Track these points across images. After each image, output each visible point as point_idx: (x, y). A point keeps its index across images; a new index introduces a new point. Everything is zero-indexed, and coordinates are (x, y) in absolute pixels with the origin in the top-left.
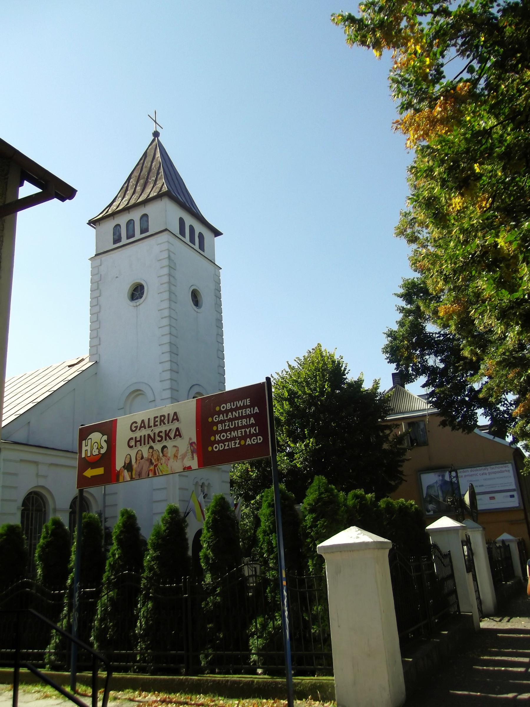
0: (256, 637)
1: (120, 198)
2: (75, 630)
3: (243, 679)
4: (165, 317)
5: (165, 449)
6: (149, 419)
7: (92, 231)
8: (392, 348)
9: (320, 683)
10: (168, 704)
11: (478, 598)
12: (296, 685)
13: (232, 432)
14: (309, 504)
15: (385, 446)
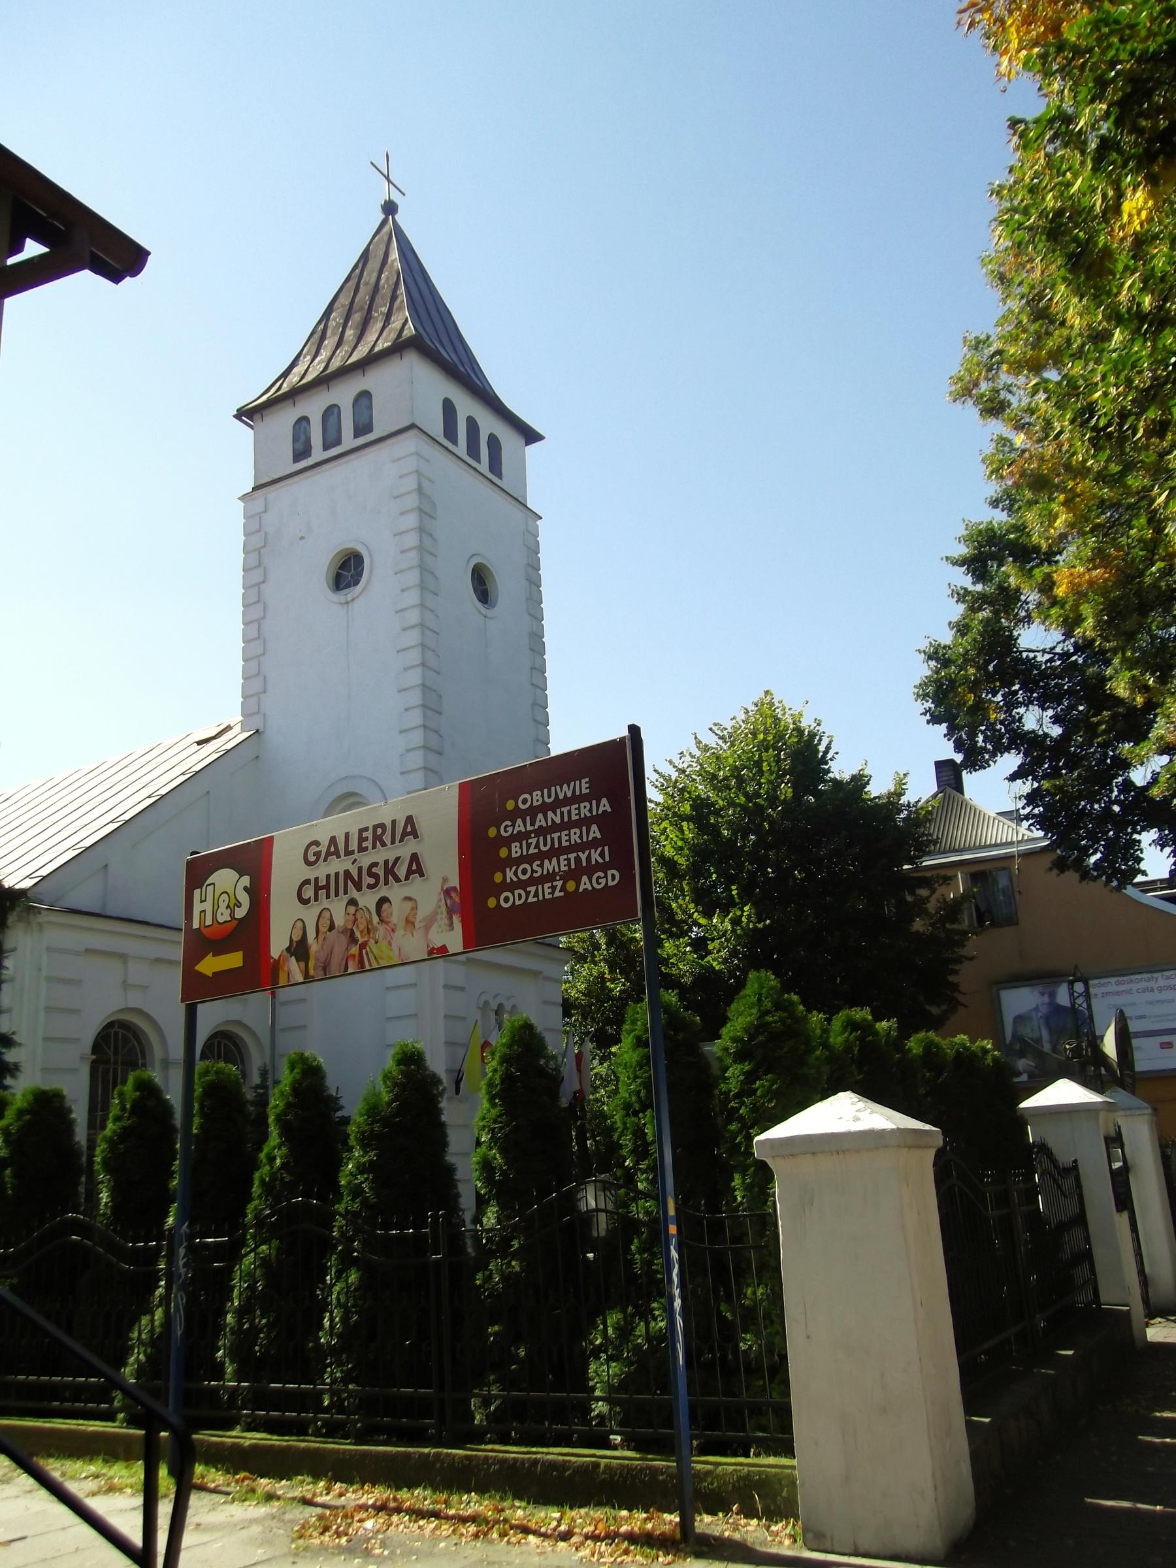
0: (603, 1356)
1: (309, 358)
2: (179, 1333)
3: (573, 1459)
4: (413, 627)
5: (385, 906)
6: (347, 835)
7: (244, 435)
8: (938, 683)
9: (760, 1473)
10: (391, 1516)
11: (1141, 1272)
12: (701, 1476)
13: (546, 861)
14: (734, 1040)
15: (918, 925)
